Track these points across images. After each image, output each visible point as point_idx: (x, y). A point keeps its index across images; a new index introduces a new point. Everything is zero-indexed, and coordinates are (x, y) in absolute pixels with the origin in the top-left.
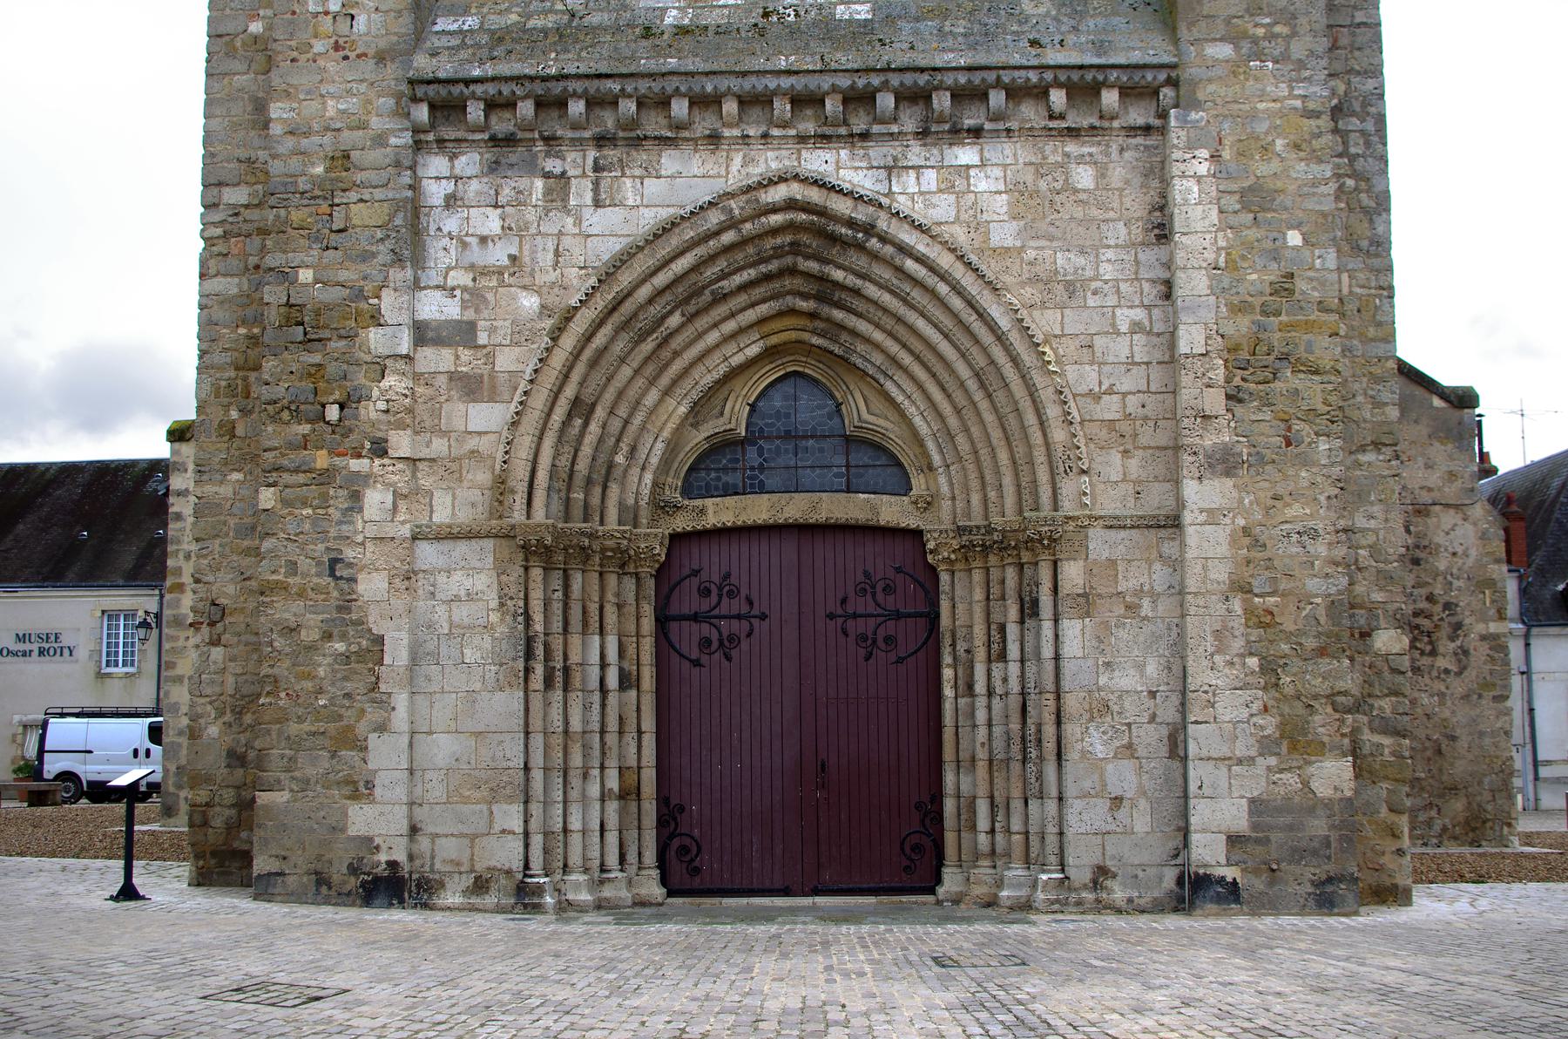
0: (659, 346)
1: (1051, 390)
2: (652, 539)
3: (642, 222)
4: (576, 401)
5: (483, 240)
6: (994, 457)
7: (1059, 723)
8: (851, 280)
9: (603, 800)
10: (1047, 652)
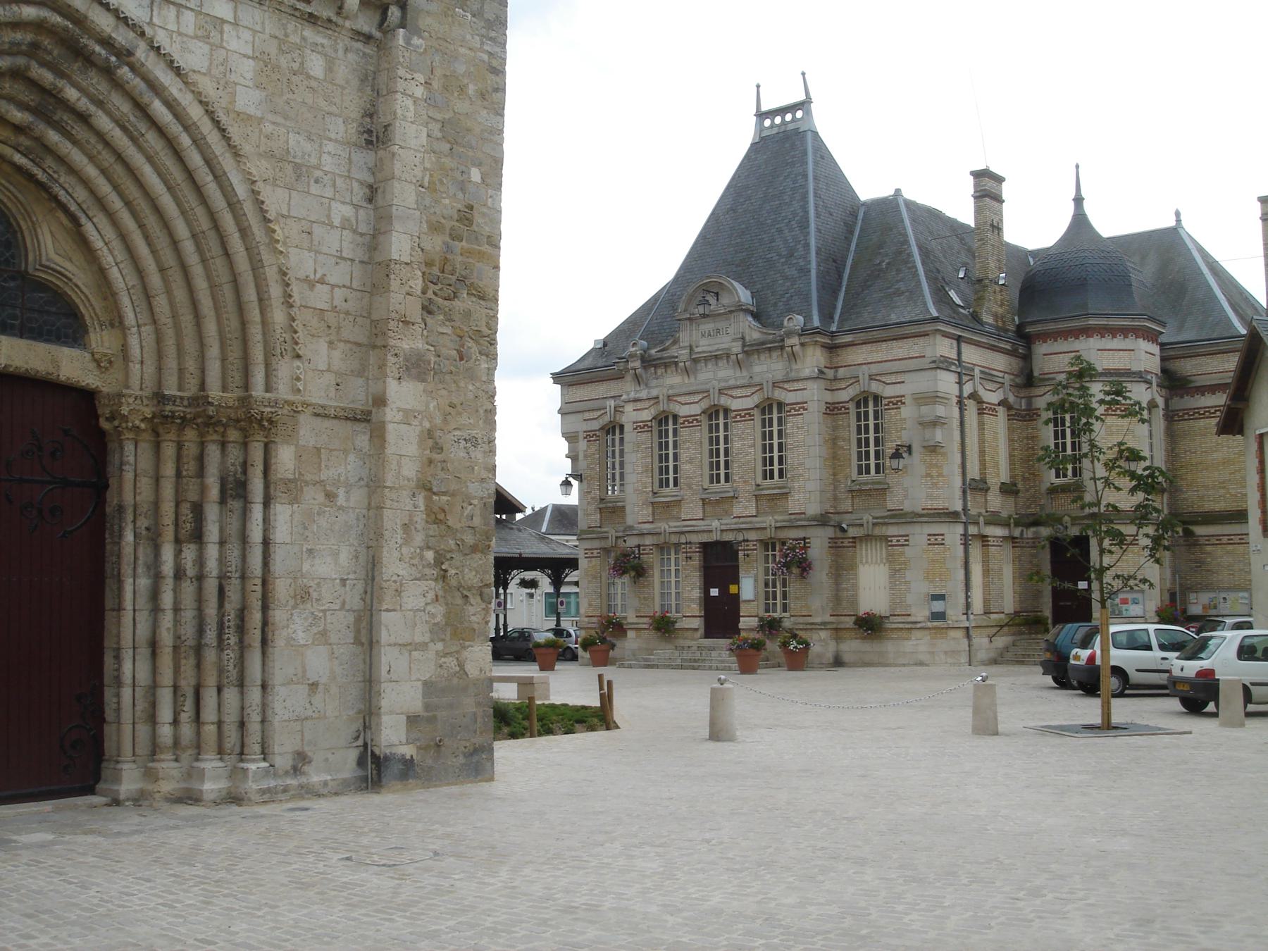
1: (275, 268)
7: (265, 608)
8: (84, 104)
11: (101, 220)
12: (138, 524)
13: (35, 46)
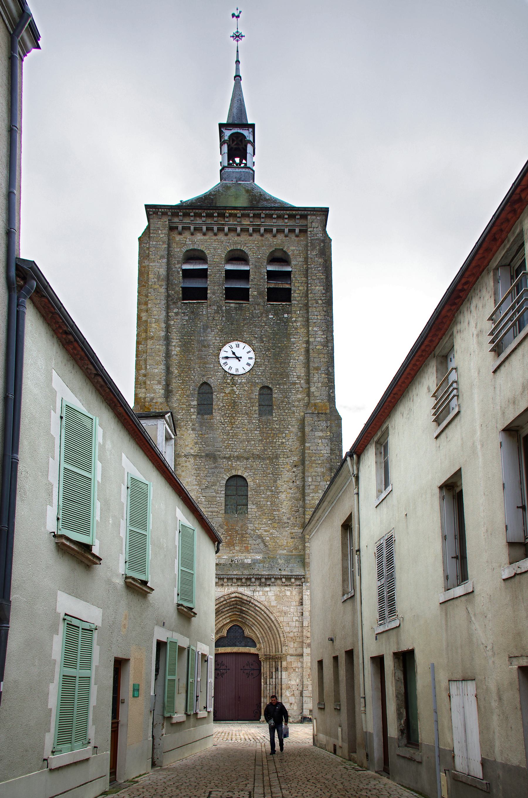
8: (246, 610)
10: (280, 677)
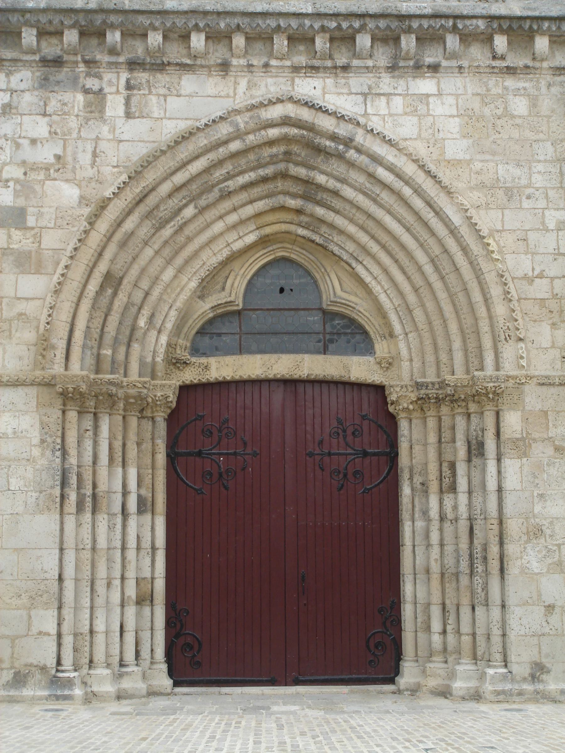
0: (176, 232)
1: (494, 273)
2: (167, 389)
3: (165, 131)
4: (108, 276)
5: (34, 142)
6: (446, 326)
7: (501, 543)
8: (332, 184)
9: (122, 606)
10: (492, 485)
11: (367, 261)
12: (415, 480)
13: (287, 153)
